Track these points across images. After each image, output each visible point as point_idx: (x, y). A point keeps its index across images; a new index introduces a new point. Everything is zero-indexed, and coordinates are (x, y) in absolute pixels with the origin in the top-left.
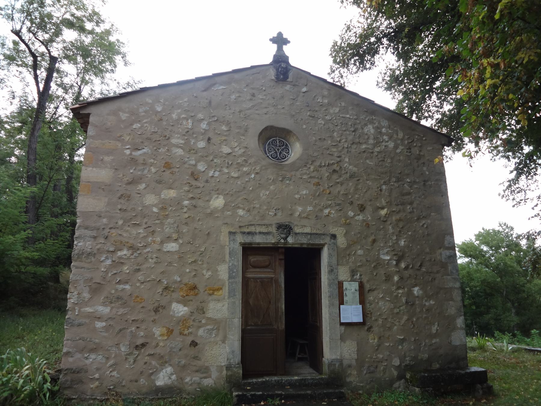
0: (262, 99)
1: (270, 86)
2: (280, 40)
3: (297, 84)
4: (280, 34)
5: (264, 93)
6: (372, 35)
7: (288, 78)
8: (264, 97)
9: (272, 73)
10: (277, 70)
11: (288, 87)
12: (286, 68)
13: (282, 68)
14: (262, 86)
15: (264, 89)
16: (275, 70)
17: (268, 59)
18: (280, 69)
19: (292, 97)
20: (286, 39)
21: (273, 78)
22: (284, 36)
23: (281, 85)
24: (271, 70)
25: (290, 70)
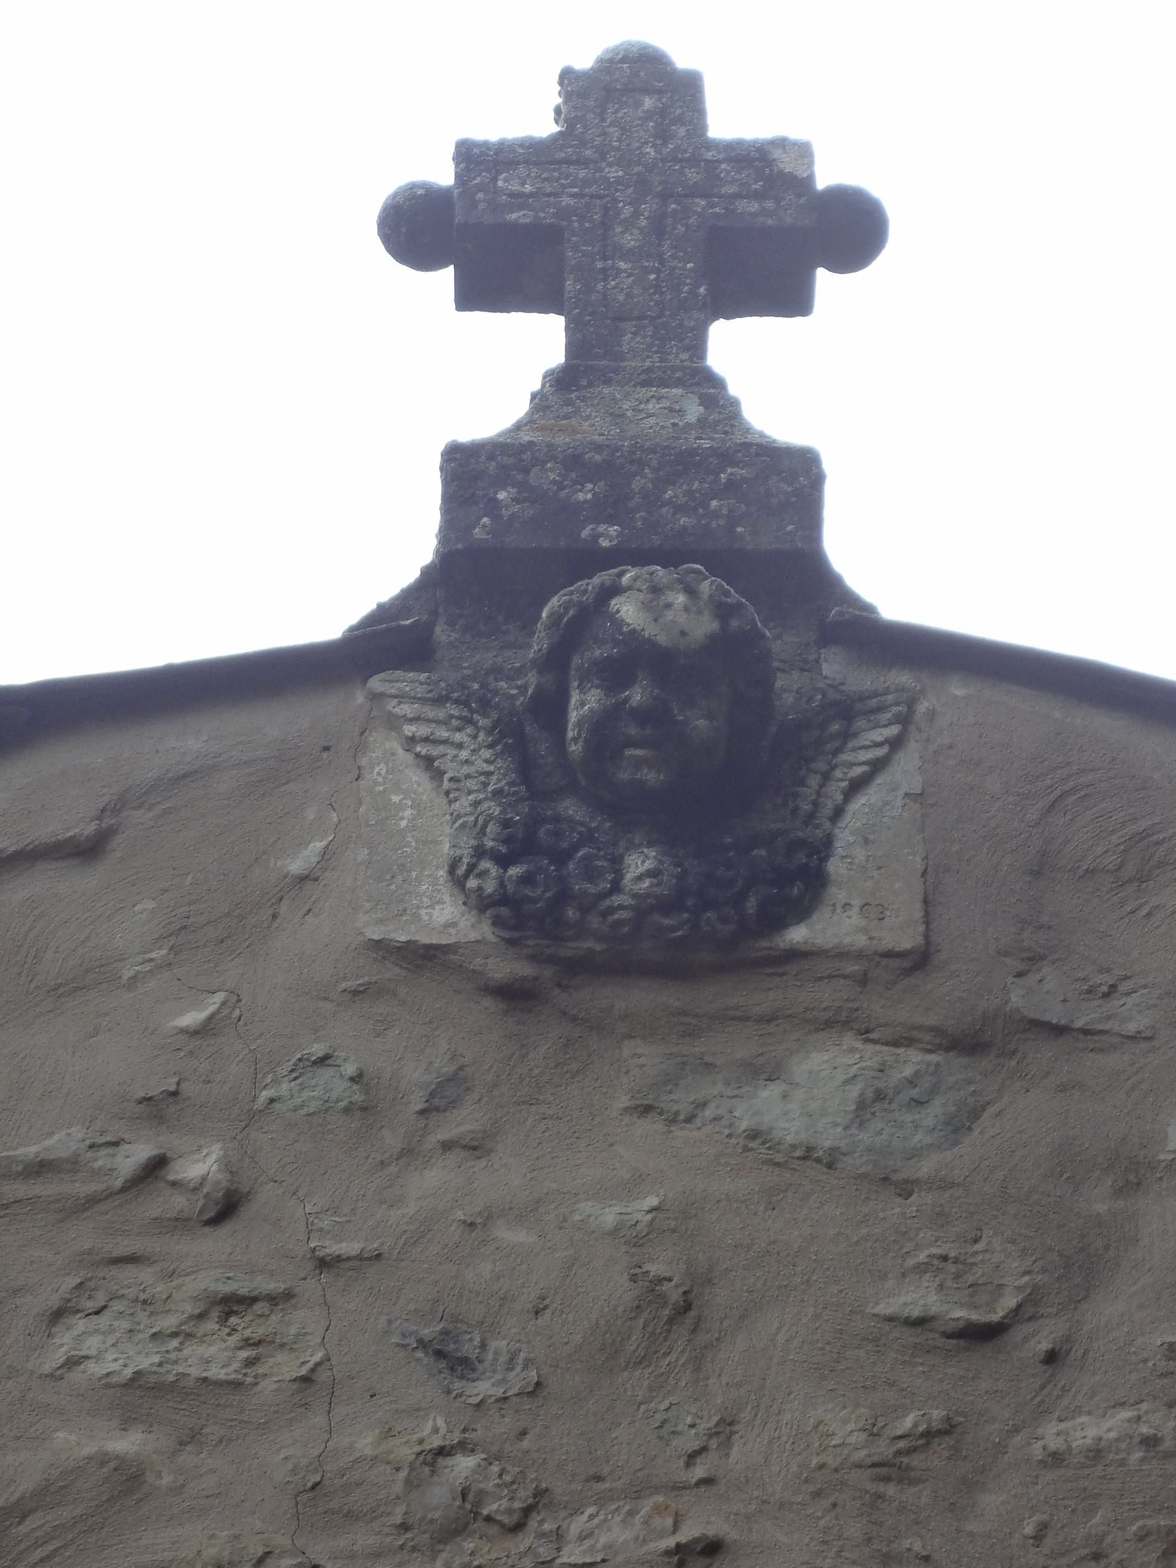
0: (138, 1395)
1: (367, 1105)
2: (635, 223)
3: (1048, 994)
4: (632, 98)
5: (212, 1263)
6: (703, 196)
7: (802, 880)
8: (213, 1355)
9: (412, 831)
10: (525, 734)
11: (814, 1090)
12: (733, 661)
13: (635, 658)
14: (159, 1108)
15: (201, 1165)
16: (473, 756)
17: (342, 548)
18: (584, 702)
19: (918, 1297)
20: (770, 169)
21: (443, 917)
22: (732, 116)
23: (644, 1059)
24: (390, 768)
25: (847, 711)
